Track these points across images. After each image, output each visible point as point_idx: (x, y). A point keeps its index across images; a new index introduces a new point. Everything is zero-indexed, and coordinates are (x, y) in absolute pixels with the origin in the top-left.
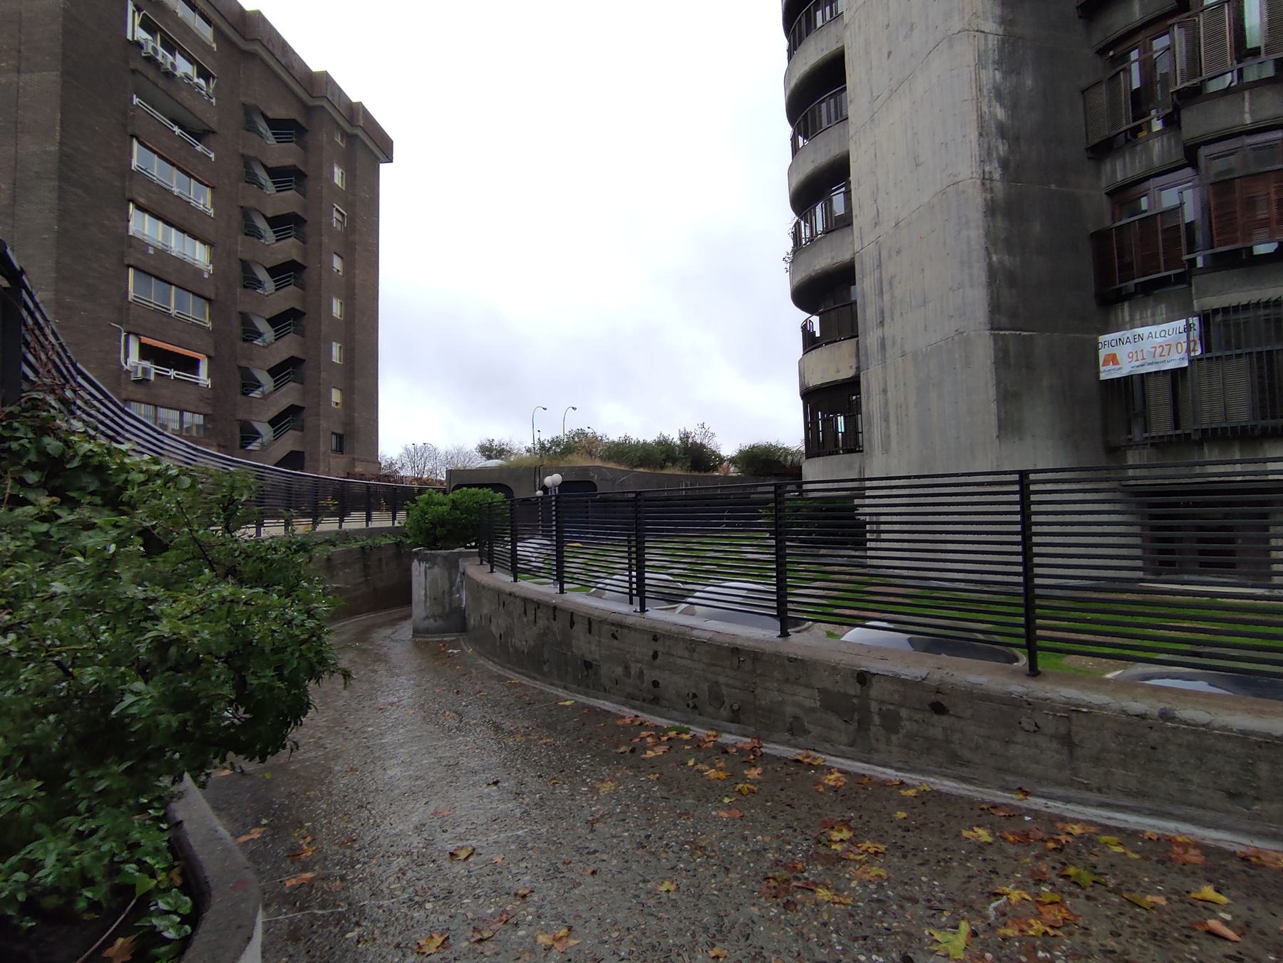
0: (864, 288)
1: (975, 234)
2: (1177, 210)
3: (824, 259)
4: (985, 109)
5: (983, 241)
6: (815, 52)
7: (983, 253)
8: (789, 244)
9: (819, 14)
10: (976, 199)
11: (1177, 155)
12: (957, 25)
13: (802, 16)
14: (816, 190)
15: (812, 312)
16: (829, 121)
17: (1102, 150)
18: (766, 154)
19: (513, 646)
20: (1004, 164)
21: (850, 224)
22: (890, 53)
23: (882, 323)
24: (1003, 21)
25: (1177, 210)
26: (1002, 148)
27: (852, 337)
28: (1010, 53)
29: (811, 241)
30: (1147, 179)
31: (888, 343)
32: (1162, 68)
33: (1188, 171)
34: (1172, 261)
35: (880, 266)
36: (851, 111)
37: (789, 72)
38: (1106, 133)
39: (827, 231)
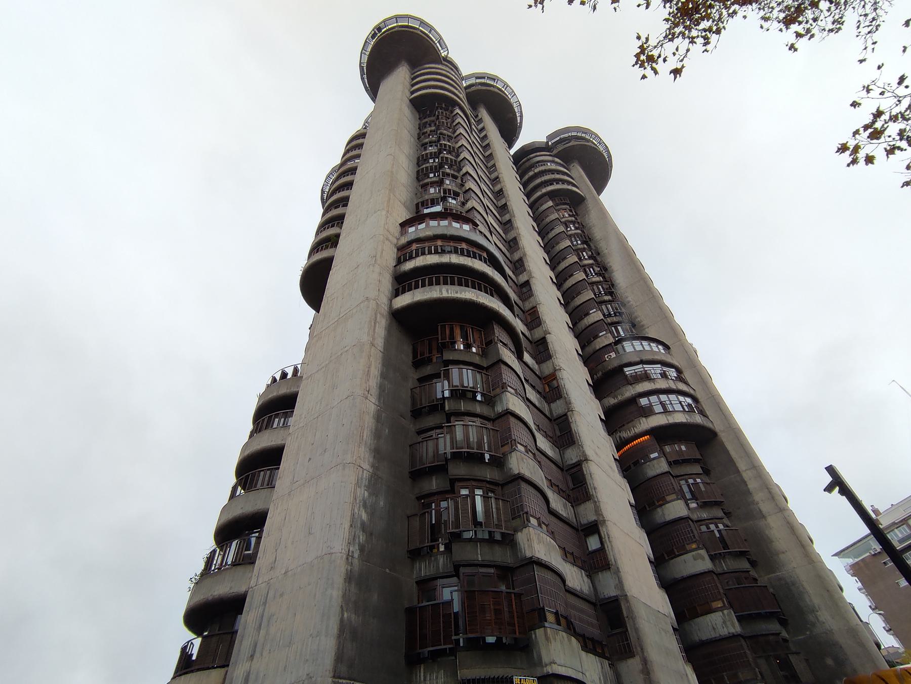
0: (247, 620)
1: (336, 594)
2: (450, 603)
3: (223, 588)
4: (356, 511)
5: (340, 600)
6: (267, 440)
7: (338, 609)
8: (201, 566)
9: (277, 420)
10: (340, 570)
11: (450, 568)
12: (349, 459)
13: (266, 418)
14: (239, 531)
15: (198, 633)
16: (262, 485)
17: (415, 554)
18: (213, 493)
19: (439, 515)
20: (362, 549)
21: (253, 563)
22: (310, 459)
23: (252, 656)
24: (373, 466)
25: (450, 603)
26: (362, 538)
27: (223, 667)
28: (373, 484)
29: (219, 569)
30: (436, 578)
31: (252, 677)
32: (444, 517)
33: (455, 579)
34: (447, 639)
35: (265, 604)
36: (278, 484)
37: (246, 446)
38: (418, 545)
39: (235, 564)
